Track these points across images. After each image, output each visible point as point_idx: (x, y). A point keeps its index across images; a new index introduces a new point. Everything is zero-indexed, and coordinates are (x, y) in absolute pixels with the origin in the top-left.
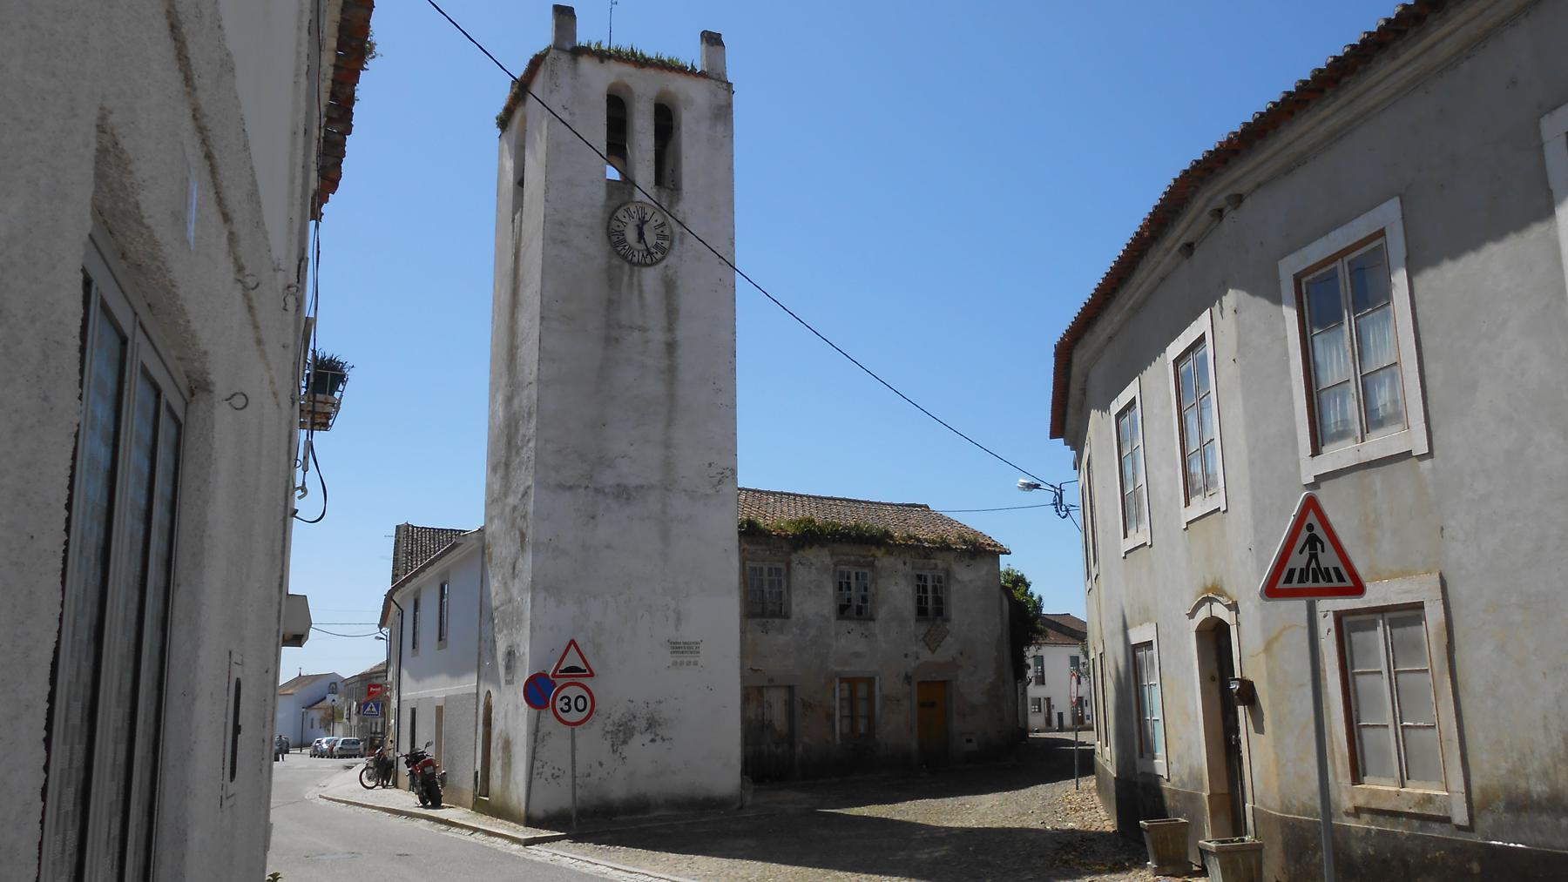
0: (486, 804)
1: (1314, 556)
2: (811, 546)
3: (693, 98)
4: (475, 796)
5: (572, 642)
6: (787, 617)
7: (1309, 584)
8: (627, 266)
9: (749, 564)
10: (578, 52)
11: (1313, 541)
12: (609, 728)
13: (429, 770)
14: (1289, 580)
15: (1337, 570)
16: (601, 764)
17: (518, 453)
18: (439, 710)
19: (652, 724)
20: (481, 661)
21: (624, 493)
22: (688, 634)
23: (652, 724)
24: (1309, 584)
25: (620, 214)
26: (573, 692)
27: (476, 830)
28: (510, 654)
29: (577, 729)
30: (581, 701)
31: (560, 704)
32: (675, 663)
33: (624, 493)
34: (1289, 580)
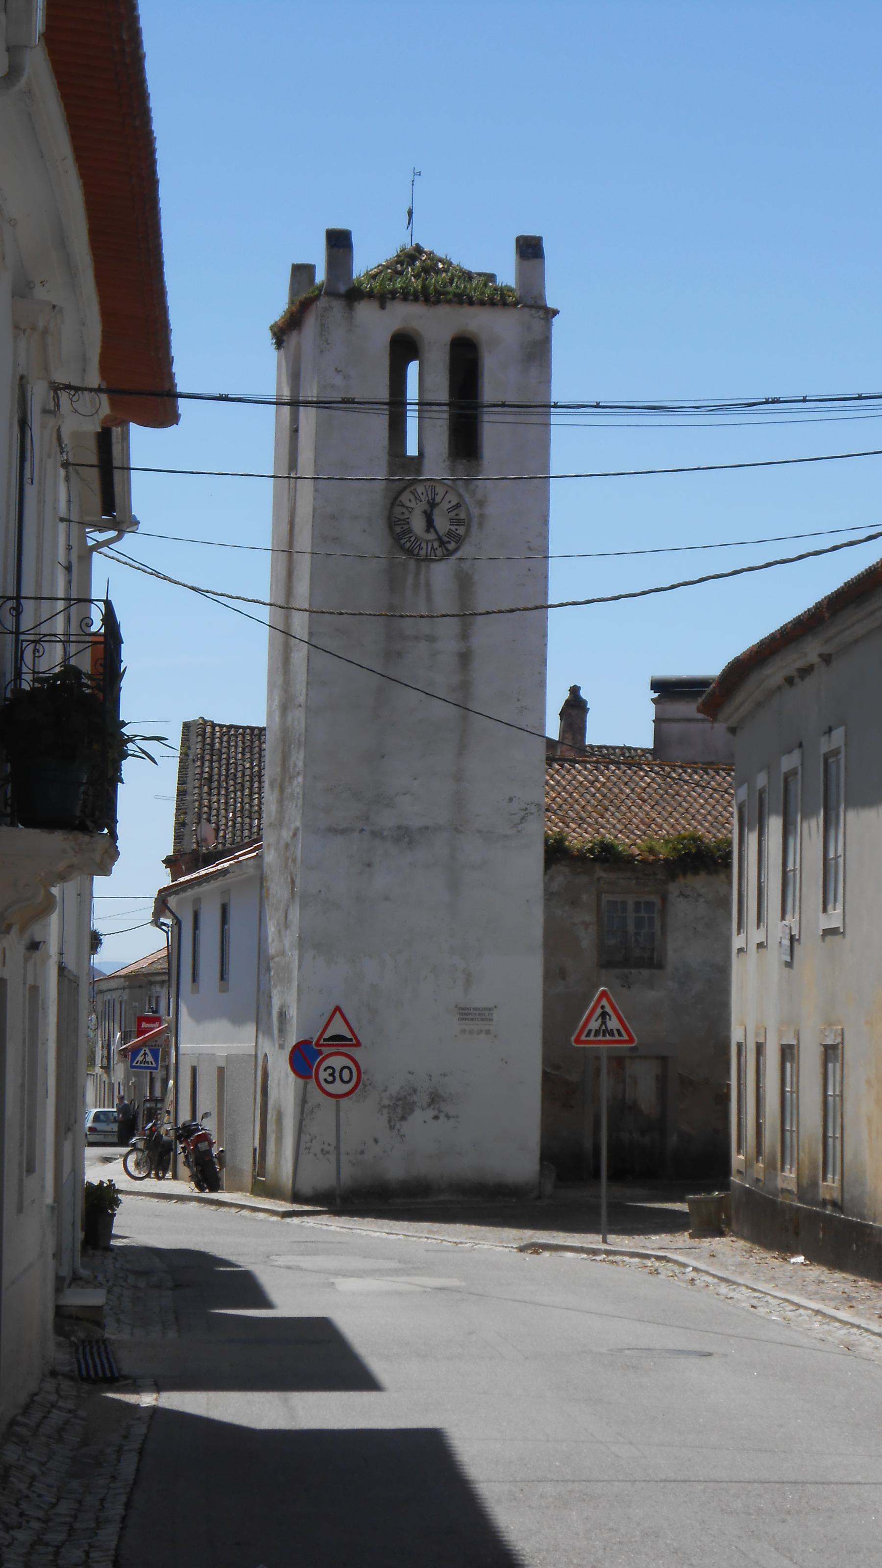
0: (264, 1188)
1: (604, 1023)
2: (696, 872)
3: (497, 330)
4: (254, 1177)
5: (338, 1009)
6: (660, 966)
7: (600, 1038)
8: (412, 564)
9: (606, 898)
10: (354, 295)
11: (604, 1015)
12: (386, 1102)
13: (203, 1146)
14: (588, 1035)
15: (618, 1030)
16: (376, 1141)
17: (290, 782)
18: (221, 1071)
19: (435, 1099)
20: (259, 1013)
21: (405, 836)
22: (479, 998)
23: (435, 1099)
24: (600, 1038)
25: (405, 497)
26: (337, 1062)
27: (243, 1207)
28: (282, 1015)
29: (344, 1102)
30: (346, 1071)
31: (323, 1075)
32: (463, 1031)
33: (405, 836)
34: (588, 1035)
